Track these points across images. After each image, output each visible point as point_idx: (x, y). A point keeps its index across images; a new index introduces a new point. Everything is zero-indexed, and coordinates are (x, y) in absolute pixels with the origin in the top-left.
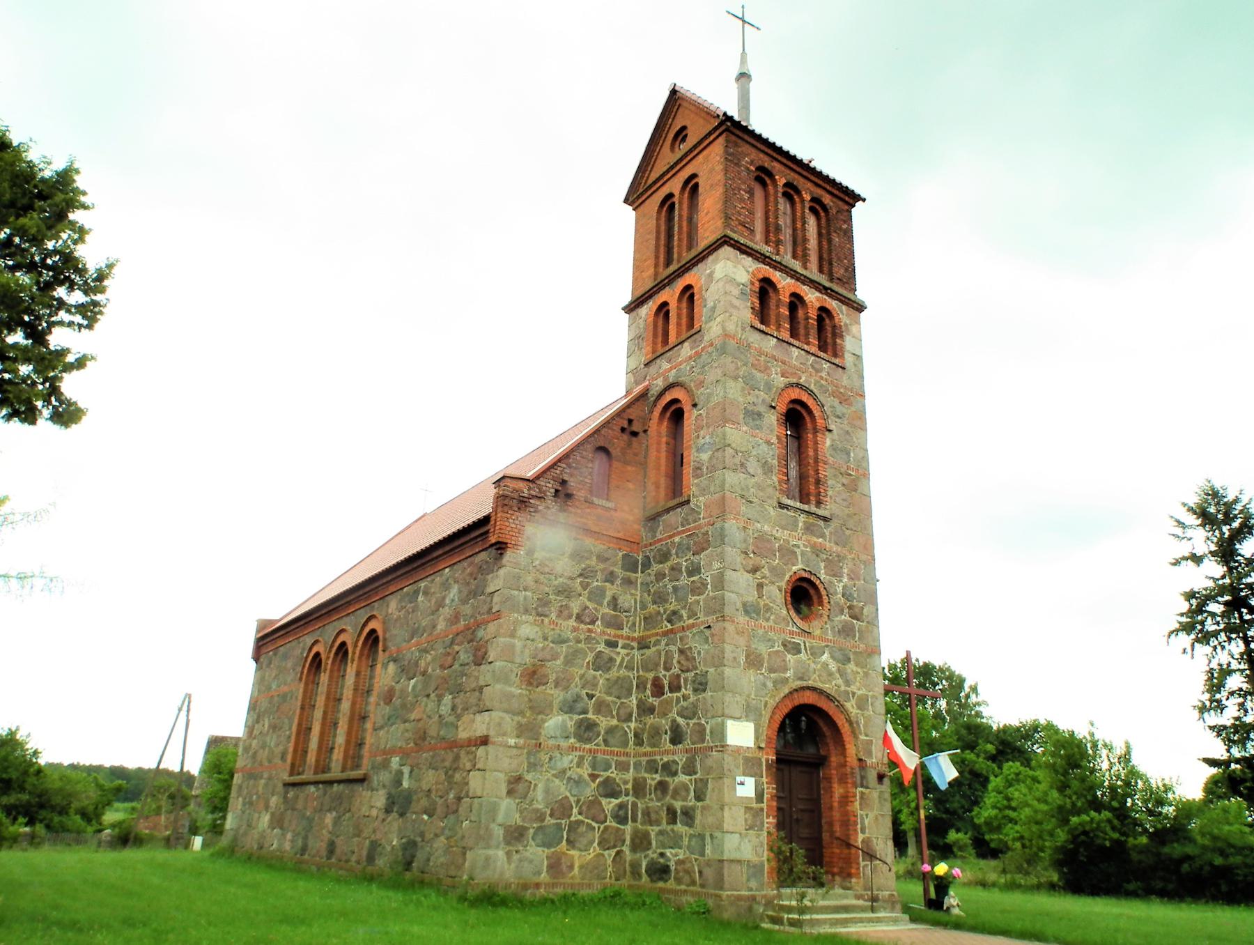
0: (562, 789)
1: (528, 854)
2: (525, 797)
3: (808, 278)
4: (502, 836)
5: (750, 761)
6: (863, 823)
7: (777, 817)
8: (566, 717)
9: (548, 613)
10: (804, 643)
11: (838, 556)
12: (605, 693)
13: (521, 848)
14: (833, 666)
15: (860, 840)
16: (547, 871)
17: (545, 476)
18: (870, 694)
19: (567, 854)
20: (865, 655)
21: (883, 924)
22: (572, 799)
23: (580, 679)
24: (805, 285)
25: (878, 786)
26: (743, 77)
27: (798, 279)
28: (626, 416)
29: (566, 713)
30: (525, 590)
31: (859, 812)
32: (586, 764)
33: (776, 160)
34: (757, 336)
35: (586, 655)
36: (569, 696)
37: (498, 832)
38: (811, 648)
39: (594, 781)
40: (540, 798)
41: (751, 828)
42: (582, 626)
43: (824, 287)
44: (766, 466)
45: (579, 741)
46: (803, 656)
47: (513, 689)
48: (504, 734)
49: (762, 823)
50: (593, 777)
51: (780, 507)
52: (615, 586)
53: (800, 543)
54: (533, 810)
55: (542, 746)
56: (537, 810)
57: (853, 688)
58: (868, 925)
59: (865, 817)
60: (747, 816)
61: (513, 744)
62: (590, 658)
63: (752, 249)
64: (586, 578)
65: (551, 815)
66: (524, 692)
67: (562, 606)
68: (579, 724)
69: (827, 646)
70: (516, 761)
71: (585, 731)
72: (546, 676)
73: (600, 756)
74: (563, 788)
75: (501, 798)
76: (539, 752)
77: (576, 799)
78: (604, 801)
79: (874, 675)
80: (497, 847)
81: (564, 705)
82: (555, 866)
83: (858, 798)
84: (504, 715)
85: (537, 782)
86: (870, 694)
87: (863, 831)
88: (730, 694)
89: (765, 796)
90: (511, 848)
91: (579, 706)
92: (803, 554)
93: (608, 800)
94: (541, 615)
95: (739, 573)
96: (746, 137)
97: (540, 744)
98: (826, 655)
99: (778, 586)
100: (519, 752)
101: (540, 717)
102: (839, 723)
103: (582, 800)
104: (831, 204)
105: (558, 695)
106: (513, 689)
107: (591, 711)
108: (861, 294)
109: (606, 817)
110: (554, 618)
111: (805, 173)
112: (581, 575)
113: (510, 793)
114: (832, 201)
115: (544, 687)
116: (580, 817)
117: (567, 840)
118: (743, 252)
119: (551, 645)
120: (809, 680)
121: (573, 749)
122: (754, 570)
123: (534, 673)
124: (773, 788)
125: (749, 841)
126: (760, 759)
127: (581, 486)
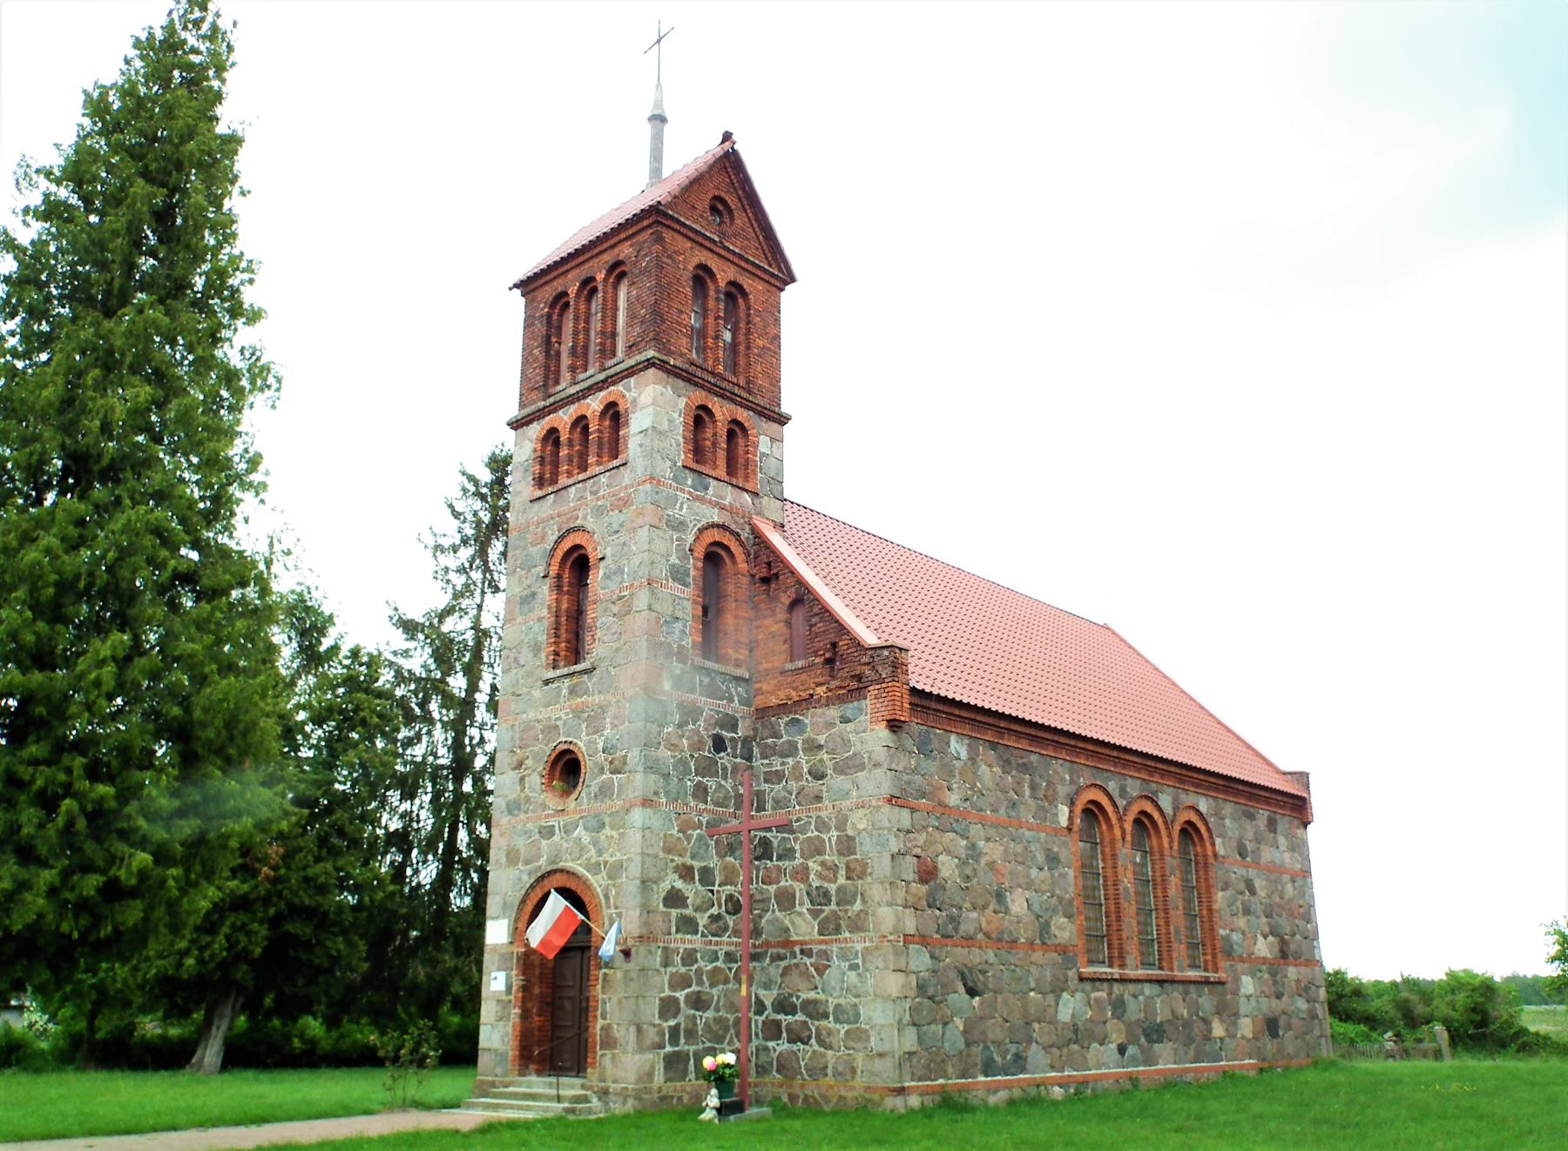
6: (604, 1009)
14: (586, 838)
27: (579, 400)
31: (601, 997)
33: (568, 271)
38: (565, 826)
43: (602, 381)
44: (536, 649)
57: (606, 857)
87: (604, 1018)
108: (785, 408)
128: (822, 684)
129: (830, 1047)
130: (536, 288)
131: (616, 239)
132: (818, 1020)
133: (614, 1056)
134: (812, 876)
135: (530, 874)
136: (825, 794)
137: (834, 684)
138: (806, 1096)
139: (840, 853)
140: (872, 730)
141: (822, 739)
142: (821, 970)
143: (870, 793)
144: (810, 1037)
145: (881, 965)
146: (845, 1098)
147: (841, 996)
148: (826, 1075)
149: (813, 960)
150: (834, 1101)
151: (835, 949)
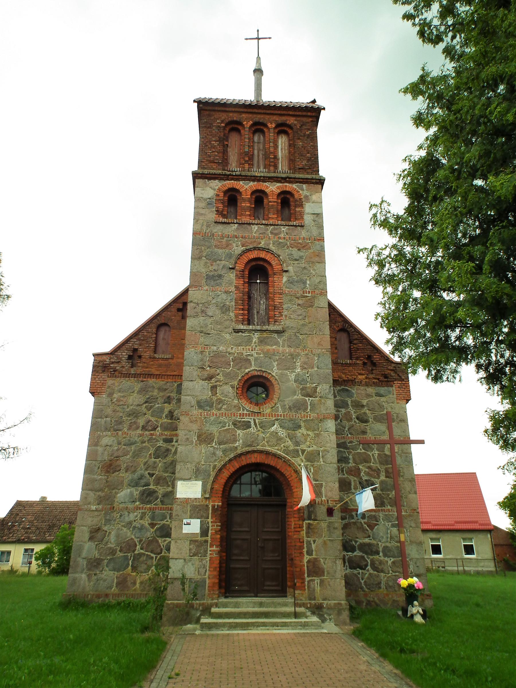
0: (129, 534)
1: (103, 576)
2: (102, 540)
3: (266, 177)
4: (85, 565)
5: (197, 508)
7: (221, 545)
8: (133, 489)
9: (121, 428)
10: (254, 420)
11: (291, 355)
12: (163, 471)
13: (98, 572)
14: (282, 433)
15: (305, 560)
16: (116, 586)
17: (122, 349)
18: (322, 449)
19: (131, 575)
20: (316, 422)
21: (290, 628)
22: (136, 540)
23: (144, 465)
24: (266, 182)
25: (327, 518)
26: (258, 72)
27: (259, 181)
28: (181, 301)
29: (133, 487)
30: (106, 417)
32: (147, 517)
34: (220, 227)
35: (149, 449)
36: (136, 476)
37: (83, 563)
39: (153, 528)
40: (112, 541)
41: (194, 555)
42: (147, 433)
43: (282, 178)
44: (224, 309)
45: (142, 504)
46: (253, 429)
47: (96, 476)
48: (89, 504)
49: (206, 551)
50: (152, 525)
51: (235, 332)
52: (171, 405)
53: (253, 352)
54: (108, 548)
55: (115, 509)
56: (110, 548)
57: (303, 447)
58: (271, 628)
59: (312, 542)
60: (191, 547)
61: (94, 509)
62: (152, 451)
63: (215, 174)
64: (150, 403)
65: (120, 551)
66: (103, 477)
67: (131, 423)
68: (142, 493)
69: (277, 420)
70: (96, 519)
71: (147, 497)
72: (120, 466)
73: (157, 512)
74: (129, 534)
75: (85, 542)
76: (113, 512)
77: (139, 539)
78: (160, 540)
79: (326, 435)
80: (82, 572)
81: (132, 482)
82: (122, 583)
83: (304, 528)
84: (90, 492)
85: (110, 531)
86: (322, 449)
87: (309, 553)
88: (182, 464)
89: (210, 532)
90: (91, 572)
91: (143, 482)
92: (256, 359)
93: (163, 539)
94: (117, 430)
95: (195, 383)
96: (216, 108)
97: (114, 507)
98: (275, 426)
99: (231, 385)
100: (99, 513)
101: (114, 491)
102: (287, 473)
103: (144, 539)
104: (296, 122)
105: (127, 477)
106: (96, 476)
107: (152, 483)
109: (162, 550)
110: (126, 431)
111: (269, 112)
112: (146, 402)
113: (91, 538)
114: (296, 120)
115: (118, 473)
116: (142, 551)
117: (131, 566)
118: (210, 179)
119: (124, 447)
120: (258, 445)
121: (138, 508)
122: (210, 378)
123: (111, 465)
124: (217, 526)
125: (193, 564)
126: (207, 506)
127: (147, 350)
128: (363, 375)
129: (382, 571)
130: (214, 111)
131: (284, 112)
132: (371, 555)
133: (322, 582)
134: (362, 474)
135: (224, 451)
136: (368, 431)
137: (371, 376)
138: (369, 601)
139: (381, 463)
140: (398, 403)
141: (365, 402)
142: (371, 527)
143: (399, 434)
144: (366, 565)
145: (413, 525)
146: (397, 601)
147: (387, 542)
148: (380, 588)
149: (366, 521)
150: (390, 603)
151: (381, 515)
